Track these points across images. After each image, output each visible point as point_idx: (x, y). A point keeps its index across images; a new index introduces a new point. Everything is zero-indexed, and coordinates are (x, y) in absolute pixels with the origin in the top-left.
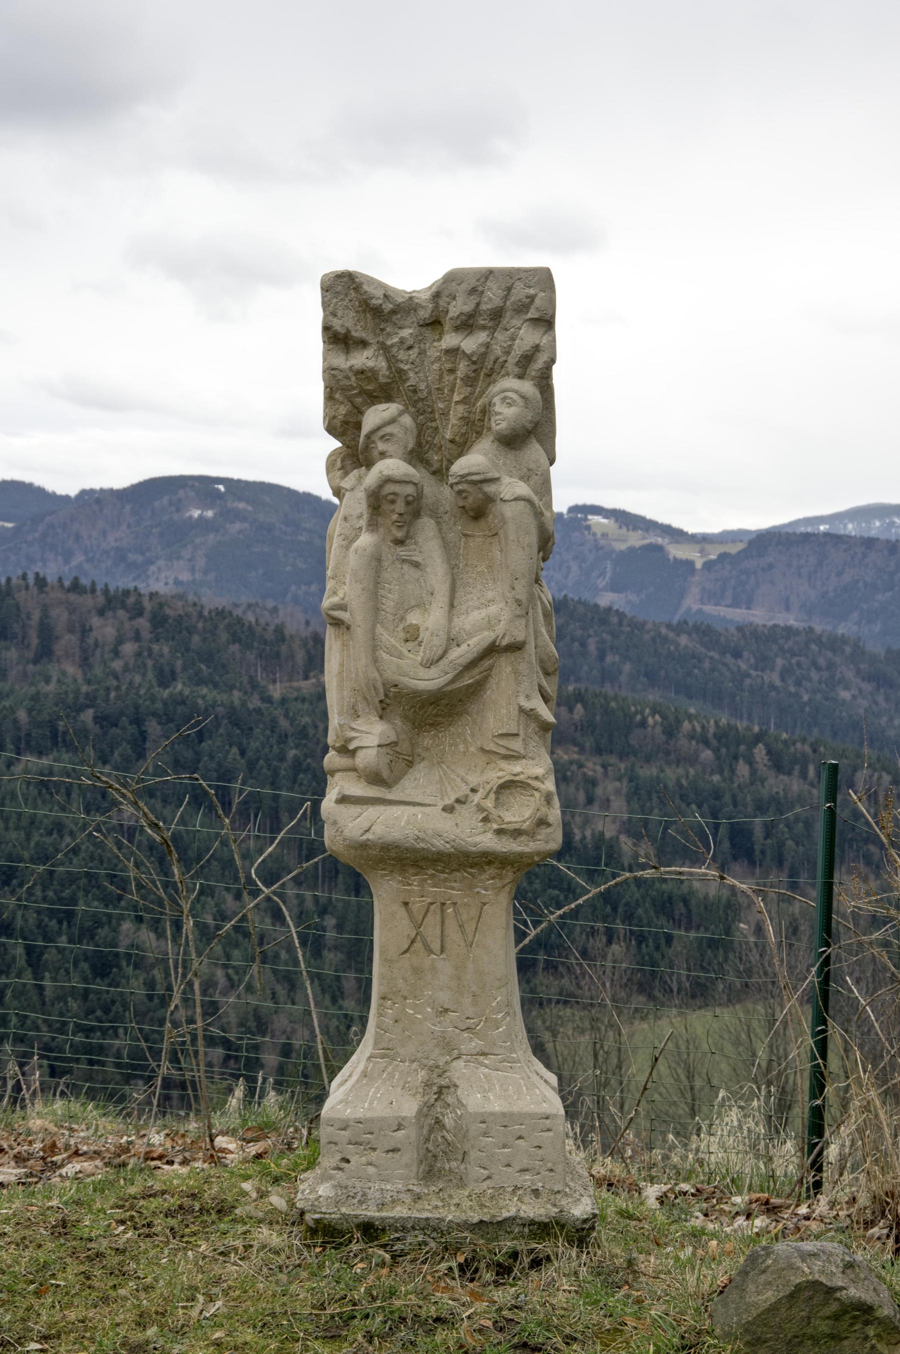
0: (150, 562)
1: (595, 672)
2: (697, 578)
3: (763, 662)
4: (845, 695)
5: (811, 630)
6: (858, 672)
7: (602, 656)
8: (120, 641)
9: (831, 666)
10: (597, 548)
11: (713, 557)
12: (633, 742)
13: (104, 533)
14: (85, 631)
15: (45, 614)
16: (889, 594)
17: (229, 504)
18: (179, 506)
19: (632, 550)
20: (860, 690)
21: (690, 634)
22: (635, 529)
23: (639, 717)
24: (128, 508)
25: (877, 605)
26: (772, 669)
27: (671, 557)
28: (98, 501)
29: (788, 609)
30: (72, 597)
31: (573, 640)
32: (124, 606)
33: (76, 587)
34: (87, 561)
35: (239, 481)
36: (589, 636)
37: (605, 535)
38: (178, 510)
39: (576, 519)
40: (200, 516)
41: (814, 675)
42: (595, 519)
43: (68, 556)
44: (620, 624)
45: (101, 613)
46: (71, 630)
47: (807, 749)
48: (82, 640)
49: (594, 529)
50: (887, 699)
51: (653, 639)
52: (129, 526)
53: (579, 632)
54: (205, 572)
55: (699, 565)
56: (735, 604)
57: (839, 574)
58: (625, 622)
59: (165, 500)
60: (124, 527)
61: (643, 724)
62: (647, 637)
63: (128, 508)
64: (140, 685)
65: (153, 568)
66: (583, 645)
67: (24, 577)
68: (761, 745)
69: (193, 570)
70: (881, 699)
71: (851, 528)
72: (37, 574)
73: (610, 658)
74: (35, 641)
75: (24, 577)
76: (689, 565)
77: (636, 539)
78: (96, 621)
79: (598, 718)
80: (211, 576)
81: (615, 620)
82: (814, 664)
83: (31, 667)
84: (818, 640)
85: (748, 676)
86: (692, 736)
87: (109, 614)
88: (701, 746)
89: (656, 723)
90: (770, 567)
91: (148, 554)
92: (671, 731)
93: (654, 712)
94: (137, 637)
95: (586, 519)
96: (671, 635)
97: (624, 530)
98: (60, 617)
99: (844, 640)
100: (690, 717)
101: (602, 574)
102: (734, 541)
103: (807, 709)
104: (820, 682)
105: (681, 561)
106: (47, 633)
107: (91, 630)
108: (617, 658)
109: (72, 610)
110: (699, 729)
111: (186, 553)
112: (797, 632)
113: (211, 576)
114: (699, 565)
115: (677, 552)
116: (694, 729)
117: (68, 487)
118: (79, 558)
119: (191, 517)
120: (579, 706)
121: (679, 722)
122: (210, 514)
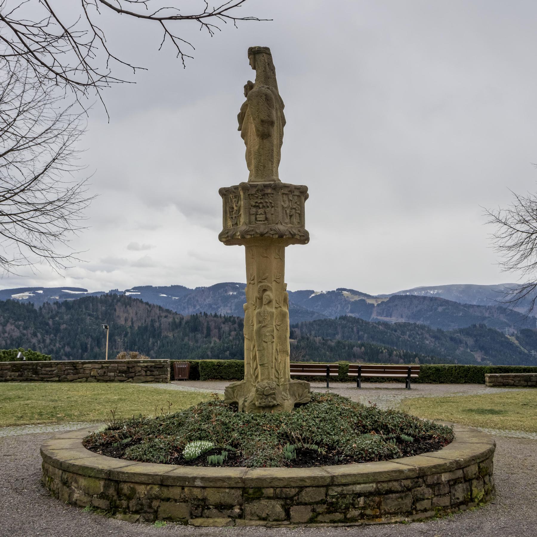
0: (219, 307)
1: (356, 337)
2: (375, 309)
3: (403, 333)
4: (427, 342)
5: (415, 324)
6: (430, 335)
7: (358, 333)
8: (230, 331)
9: (422, 334)
10: (345, 300)
11: (380, 303)
12: (380, 358)
13: (205, 300)
14: (219, 329)
15: (208, 324)
16: (431, 313)
17: (241, 290)
18: (226, 291)
19: (356, 301)
20: (431, 341)
21: (382, 325)
22: (356, 295)
23: (381, 350)
24: (211, 292)
25: (428, 316)
26: (406, 335)
27: (367, 303)
28: (203, 291)
29: (402, 317)
30: (215, 319)
31: (349, 328)
32: (230, 321)
33: (216, 316)
34: (201, 307)
35: (243, 284)
36: (354, 327)
37: (347, 297)
38: (226, 292)
39: (339, 293)
40: (232, 294)
41: (418, 337)
42: (344, 292)
43: (195, 306)
44: (362, 323)
45: (224, 323)
46: (215, 328)
47: (430, 359)
48: (219, 331)
49: (344, 295)
50: (439, 343)
51: (372, 327)
52: (212, 297)
53: (351, 325)
54: (235, 310)
55: (376, 305)
56: (387, 316)
57: (416, 307)
58: (364, 322)
59: (222, 290)
60: (210, 298)
61: (382, 352)
62: (371, 326)
63: (211, 292)
64: (239, 344)
65: (219, 309)
66: (352, 329)
67: (201, 313)
68: (417, 358)
69: (231, 310)
70: (437, 343)
71: (416, 294)
72: (204, 312)
73: (361, 333)
74: (205, 332)
75: (201, 313)
76: (373, 305)
77: (357, 298)
78: (223, 326)
79: (369, 351)
80: (236, 311)
81: (361, 321)
82: (417, 333)
83: (205, 339)
84: (418, 326)
85: (401, 337)
86: (396, 356)
87: (226, 323)
88: (400, 359)
89: (386, 352)
90: (396, 305)
91: (218, 305)
92: (390, 354)
93: (385, 349)
94: (235, 330)
95: (342, 292)
96: (377, 326)
97: (353, 295)
98: (212, 324)
99: (425, 326)
100: (395, 350)
101: (348, 308)
102: (385, 298)
103: (418, 347)
104: (420, 339)
105: (371, 304)
106: (209, 329)
107: (221, 328)
108: (363, 333)
109: (215, 322)
110: (398, 353)
111: (229, 305)
112: (412, 324)
113: (236, 311)
114: (376, 305)
115: (369, 301)
116: (397, 353)
117: (192, 286)
118: (198, 307)
119: (230, 294)
120: (363, 347)
121: (392, 351)
122: (235, 293)
